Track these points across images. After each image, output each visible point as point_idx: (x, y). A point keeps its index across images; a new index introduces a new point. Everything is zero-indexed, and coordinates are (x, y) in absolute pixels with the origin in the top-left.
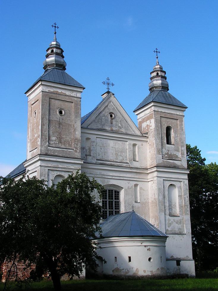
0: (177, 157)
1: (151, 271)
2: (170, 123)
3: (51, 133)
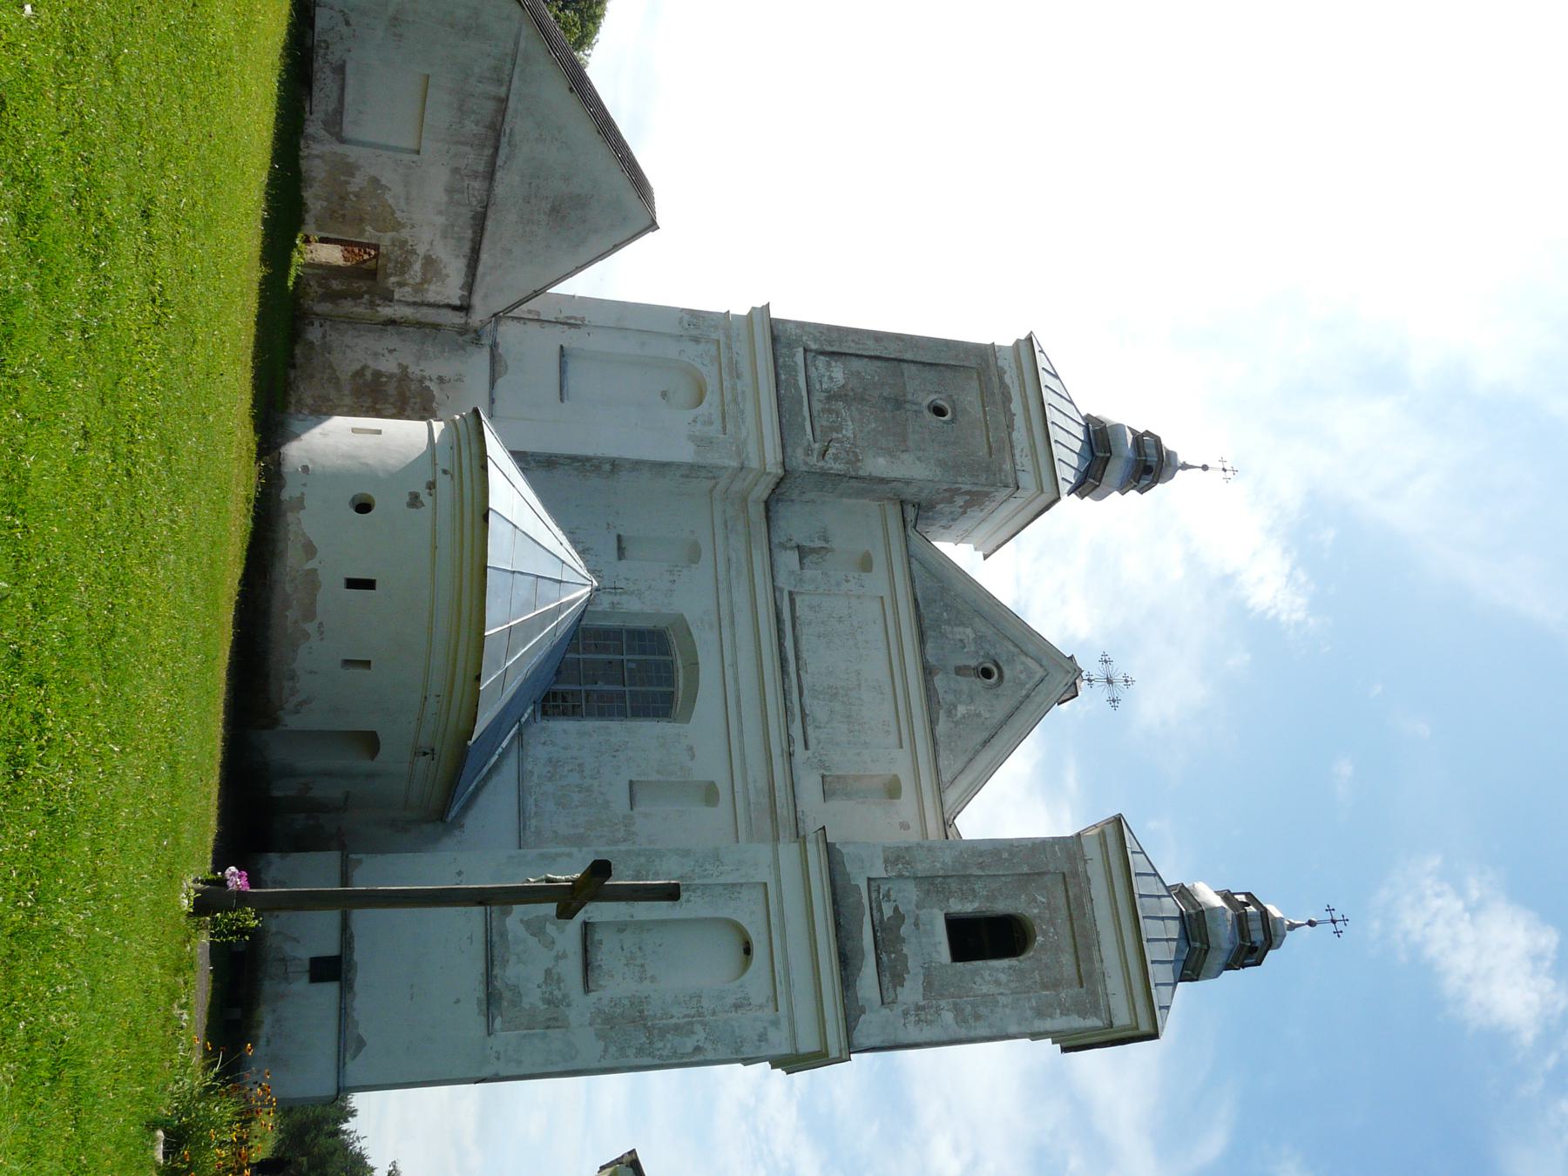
0: (899, 980)
1: (301, 499)
2: (1050, 936)
3: (856, 364)
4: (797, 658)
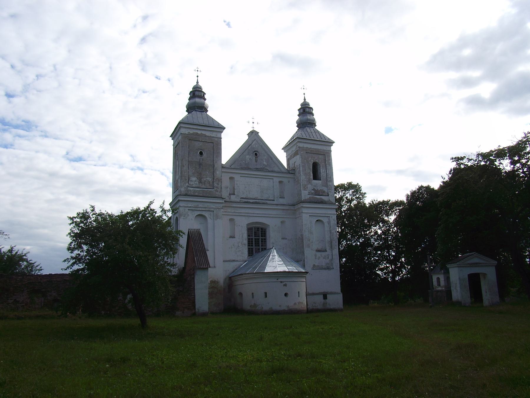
0: (324, 192)
4: (255, 199)
